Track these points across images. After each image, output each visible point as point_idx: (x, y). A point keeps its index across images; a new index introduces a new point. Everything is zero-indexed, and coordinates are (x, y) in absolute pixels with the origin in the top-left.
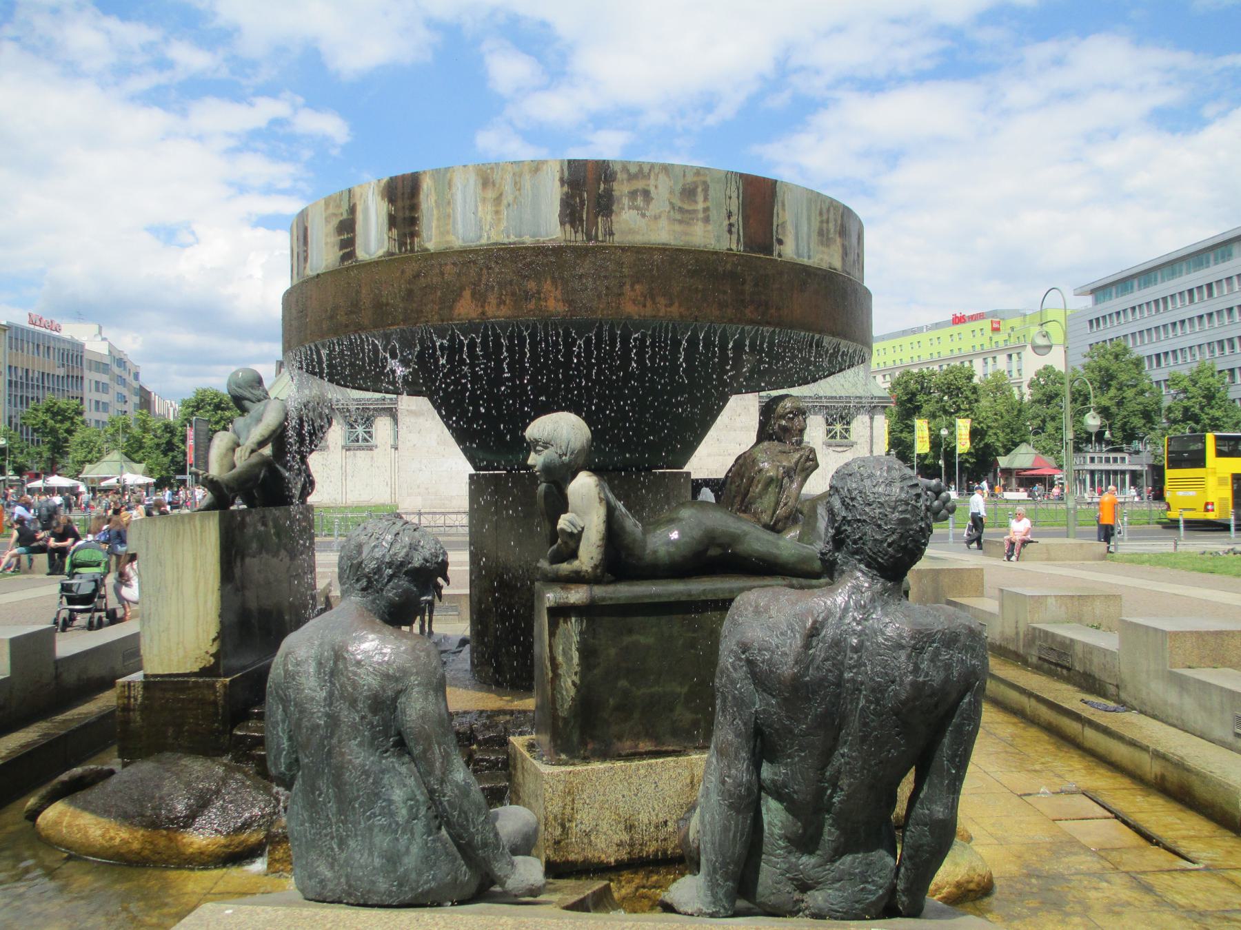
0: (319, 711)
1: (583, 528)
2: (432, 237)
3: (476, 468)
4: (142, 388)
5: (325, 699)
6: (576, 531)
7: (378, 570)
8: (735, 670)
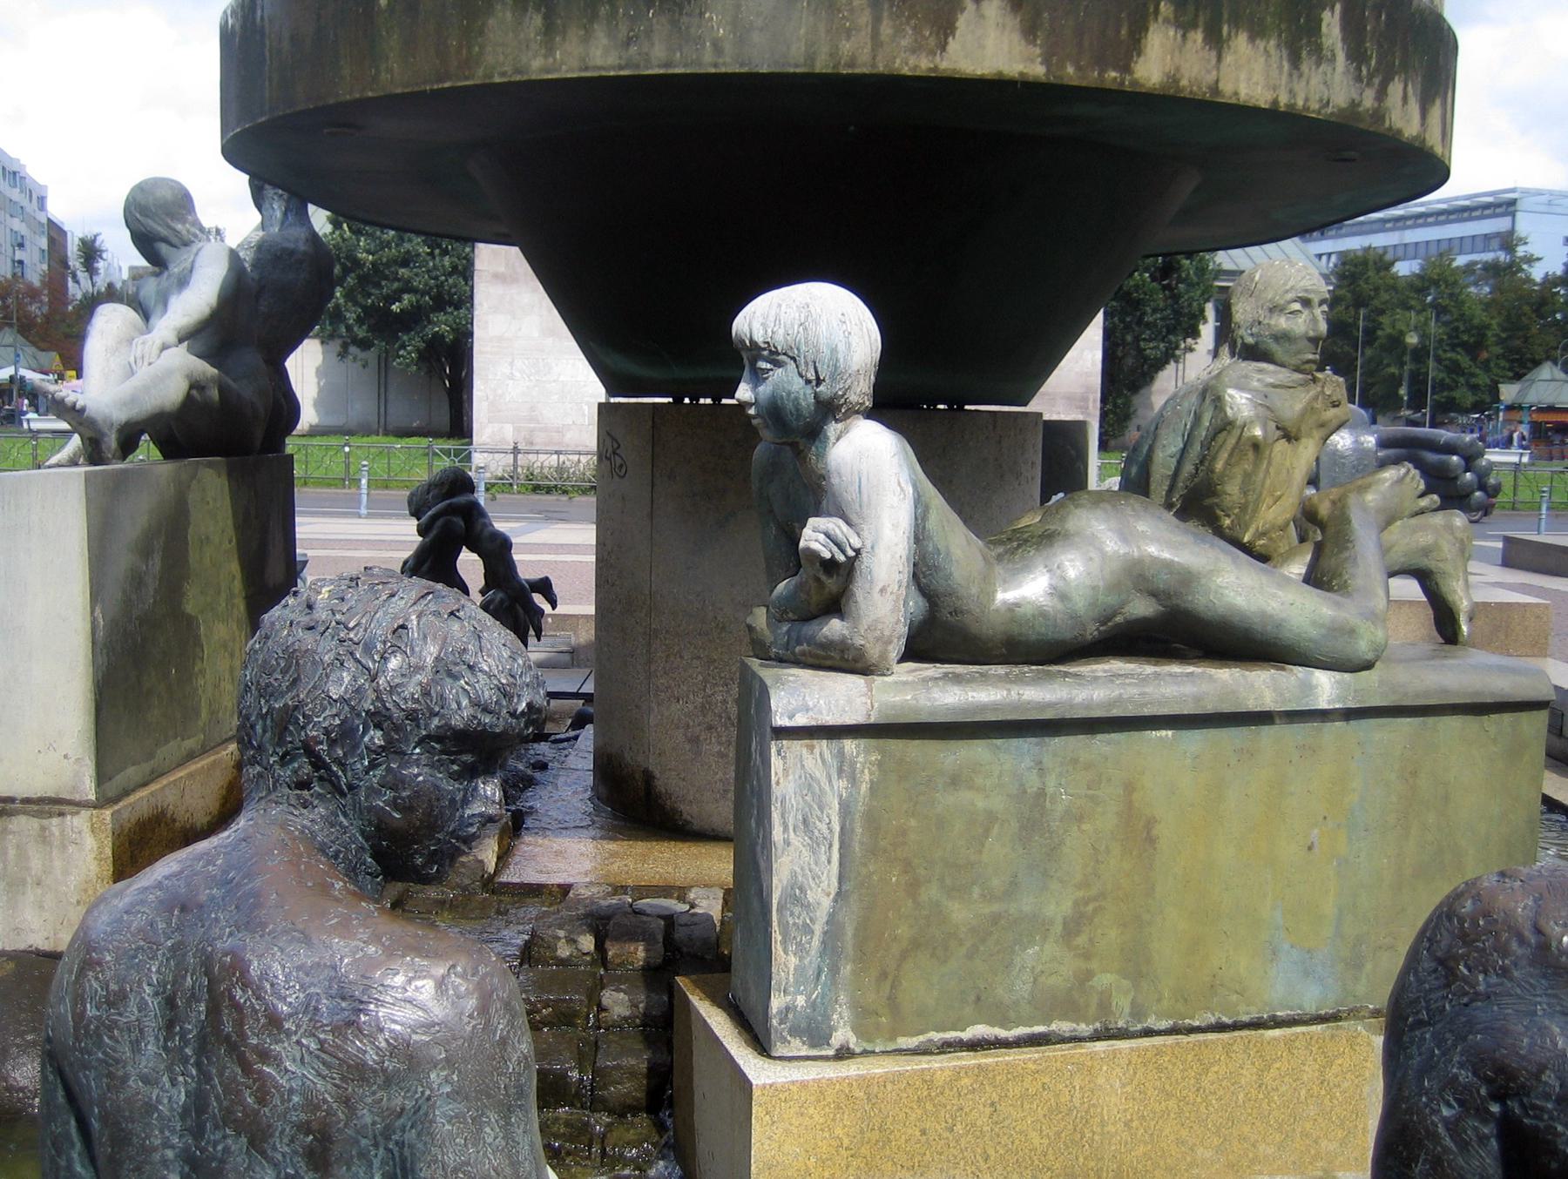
0: (167, 1144)
1: (858, 552)
2: (644, 1103)
3: (611, 392)
4: (51, 223)
5: (184, 1114)
6: (842, 558)
7: (345, 735)
8: (1464, 1146)
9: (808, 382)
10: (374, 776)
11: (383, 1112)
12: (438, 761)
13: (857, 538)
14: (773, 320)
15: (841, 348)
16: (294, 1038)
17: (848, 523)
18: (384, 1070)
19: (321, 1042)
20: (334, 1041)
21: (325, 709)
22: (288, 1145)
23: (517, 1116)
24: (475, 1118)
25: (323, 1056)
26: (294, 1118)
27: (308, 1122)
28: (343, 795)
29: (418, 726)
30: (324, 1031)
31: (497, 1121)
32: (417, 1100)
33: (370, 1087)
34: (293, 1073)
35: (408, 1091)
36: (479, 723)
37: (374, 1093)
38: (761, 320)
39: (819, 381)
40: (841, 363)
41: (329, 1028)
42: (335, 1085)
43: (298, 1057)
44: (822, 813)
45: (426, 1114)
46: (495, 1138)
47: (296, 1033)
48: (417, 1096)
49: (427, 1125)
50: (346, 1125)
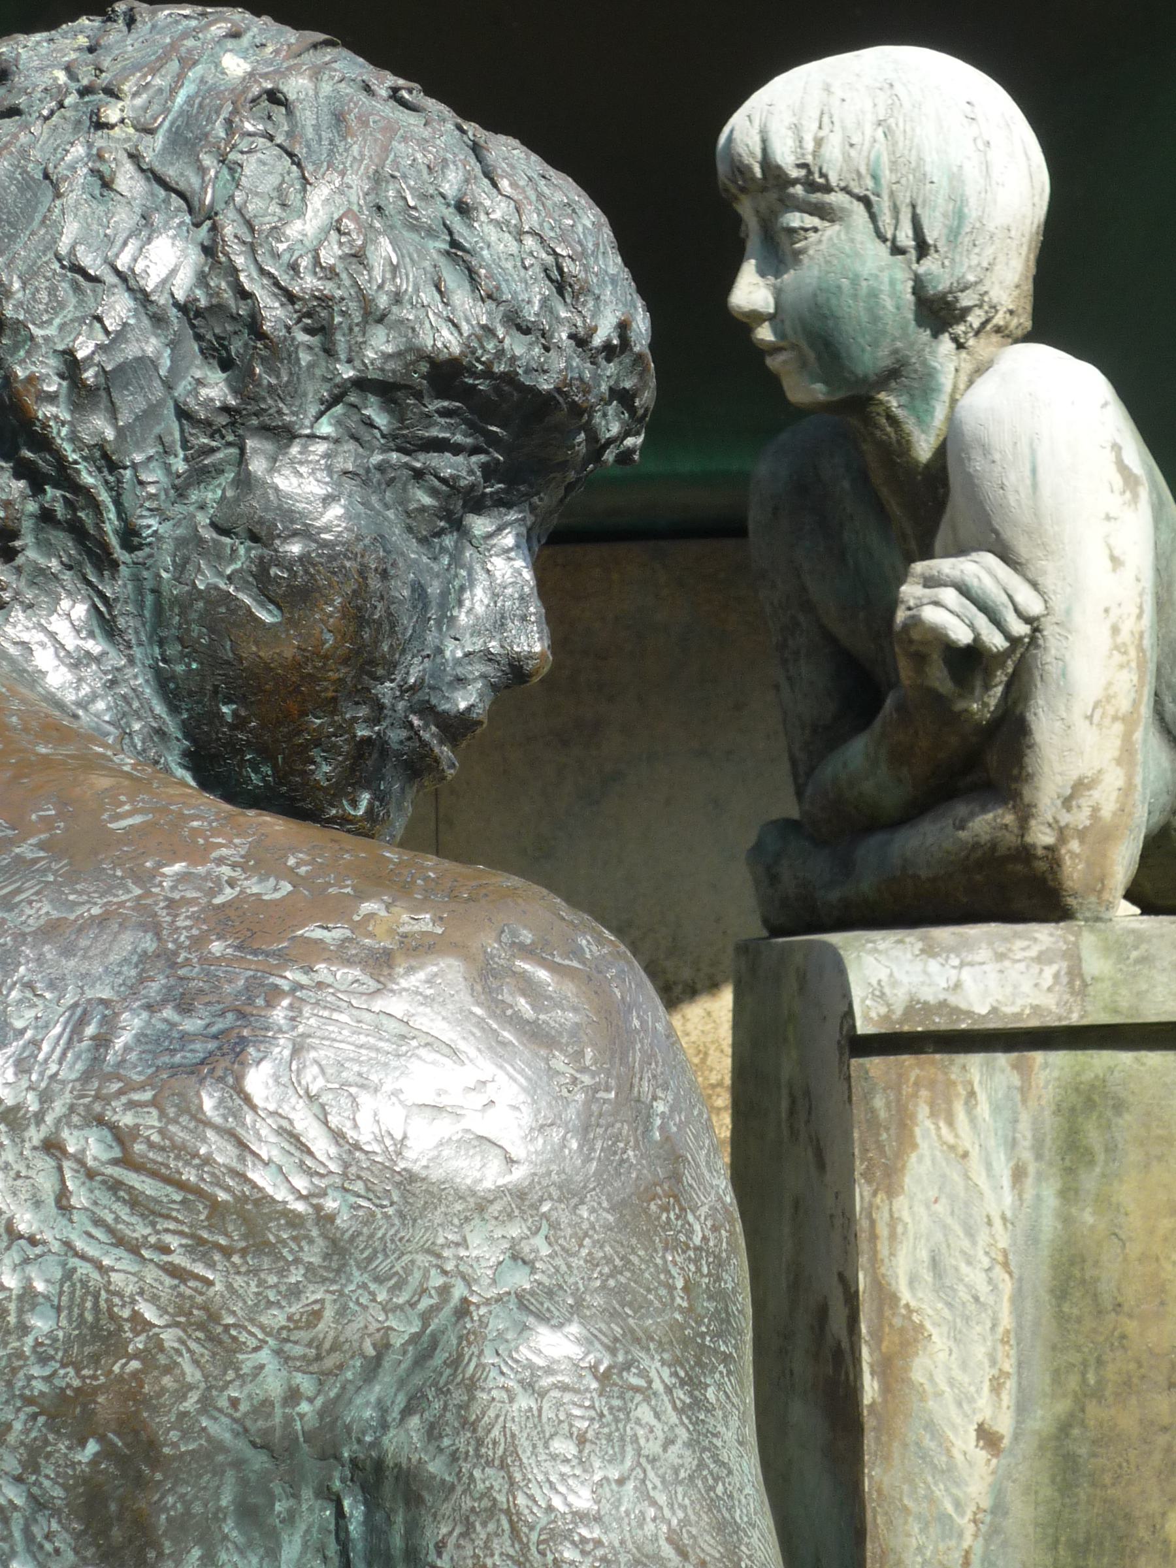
6: (996, 641)
9: (897, 250)
10: (202, 507)
11: (319, 1358)
12: (380, 468)
13: (1032, 594)
14: (815, 114)
15: (972, 174)
16: (35, 1135)
17: (1006, 556)
18: (325, 1219)
19: (121, 1137)
20: (162, 1132)
21: (62, 305)
22: (19, 1480)
23: (720, 1386)
24: (607, 1375)
25: (133, 1179)
26: (39, 1386)
27: (85, 1395)
28: (104, 562)
29: (329, 352)
30: (132, 1105)
31: (669, 1390)
32: (426, 1318)
33: (282, 1273)
34: (32, 1241)
35: (398, 1287)
36: (500, 353)
37: (295, 1292)
38: (789, 119)
39: (923, 248)
40: (972, 212)
41: (147, 1095)
42: (174, 1271)
43: (47, 1185)
44: (974, 1243)
45: (456, 1362)
46: (668, 1442)
47: (39, 1118)
48: (425, 1303)
49: (459, 1396)
50: (207, 1405)
